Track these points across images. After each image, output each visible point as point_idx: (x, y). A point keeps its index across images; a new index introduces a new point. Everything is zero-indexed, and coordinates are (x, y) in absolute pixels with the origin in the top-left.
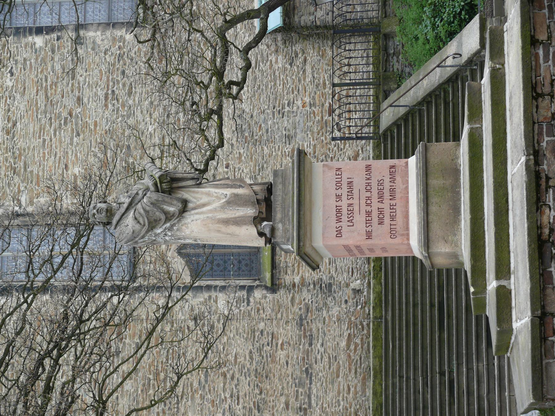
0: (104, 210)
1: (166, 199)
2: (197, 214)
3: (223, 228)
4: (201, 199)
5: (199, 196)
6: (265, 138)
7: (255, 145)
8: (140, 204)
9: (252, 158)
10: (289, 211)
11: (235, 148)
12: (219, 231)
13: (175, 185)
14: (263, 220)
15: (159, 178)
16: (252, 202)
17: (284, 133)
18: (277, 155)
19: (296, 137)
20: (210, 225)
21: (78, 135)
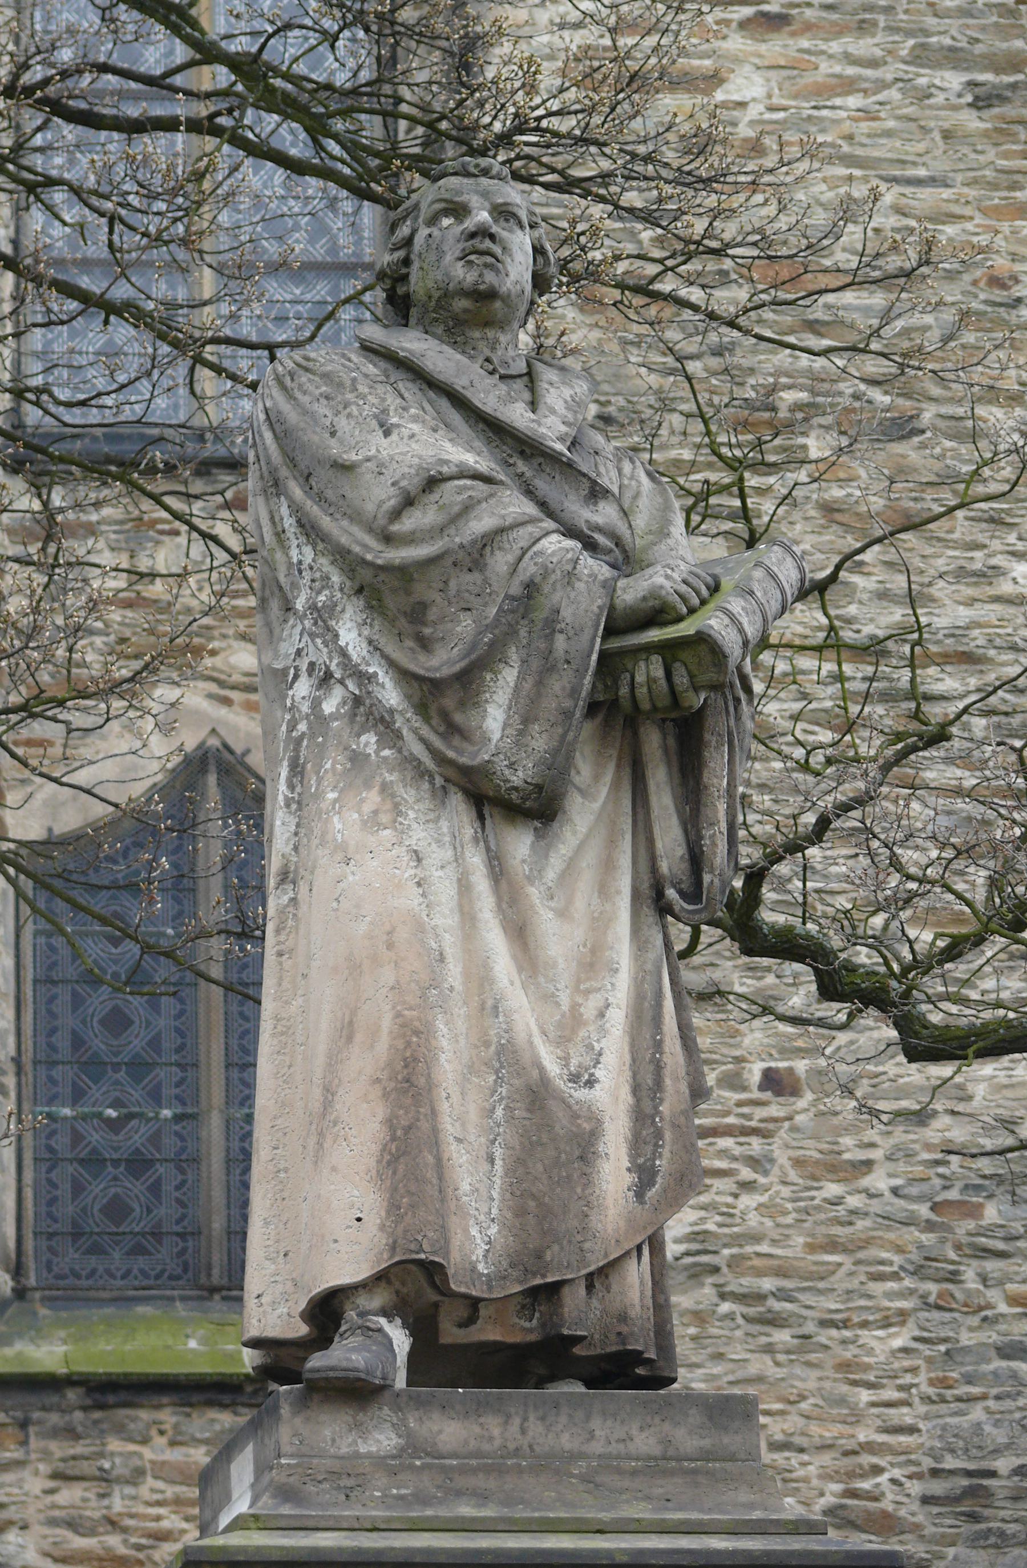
0: (490, 277)
1: (558, 685)
2: (464, 887)
3: (367, 1061)
4: (563, 914)
5: (580, 904)
6: (966, 1339)
7: (918, 1272)
8: (531, 509)
9: (832, 1245)
10: (482, 1497)
11: (900, 1135)
12: (346, 1032)
13: (653, 741)
14: (423, 1330)
15: (702, 639)
16: (539, 1255)
17: (1003, 1465)
18: (856, 1418)
19: (975, 1541)
20: (388, 976)
21: (983, 100)
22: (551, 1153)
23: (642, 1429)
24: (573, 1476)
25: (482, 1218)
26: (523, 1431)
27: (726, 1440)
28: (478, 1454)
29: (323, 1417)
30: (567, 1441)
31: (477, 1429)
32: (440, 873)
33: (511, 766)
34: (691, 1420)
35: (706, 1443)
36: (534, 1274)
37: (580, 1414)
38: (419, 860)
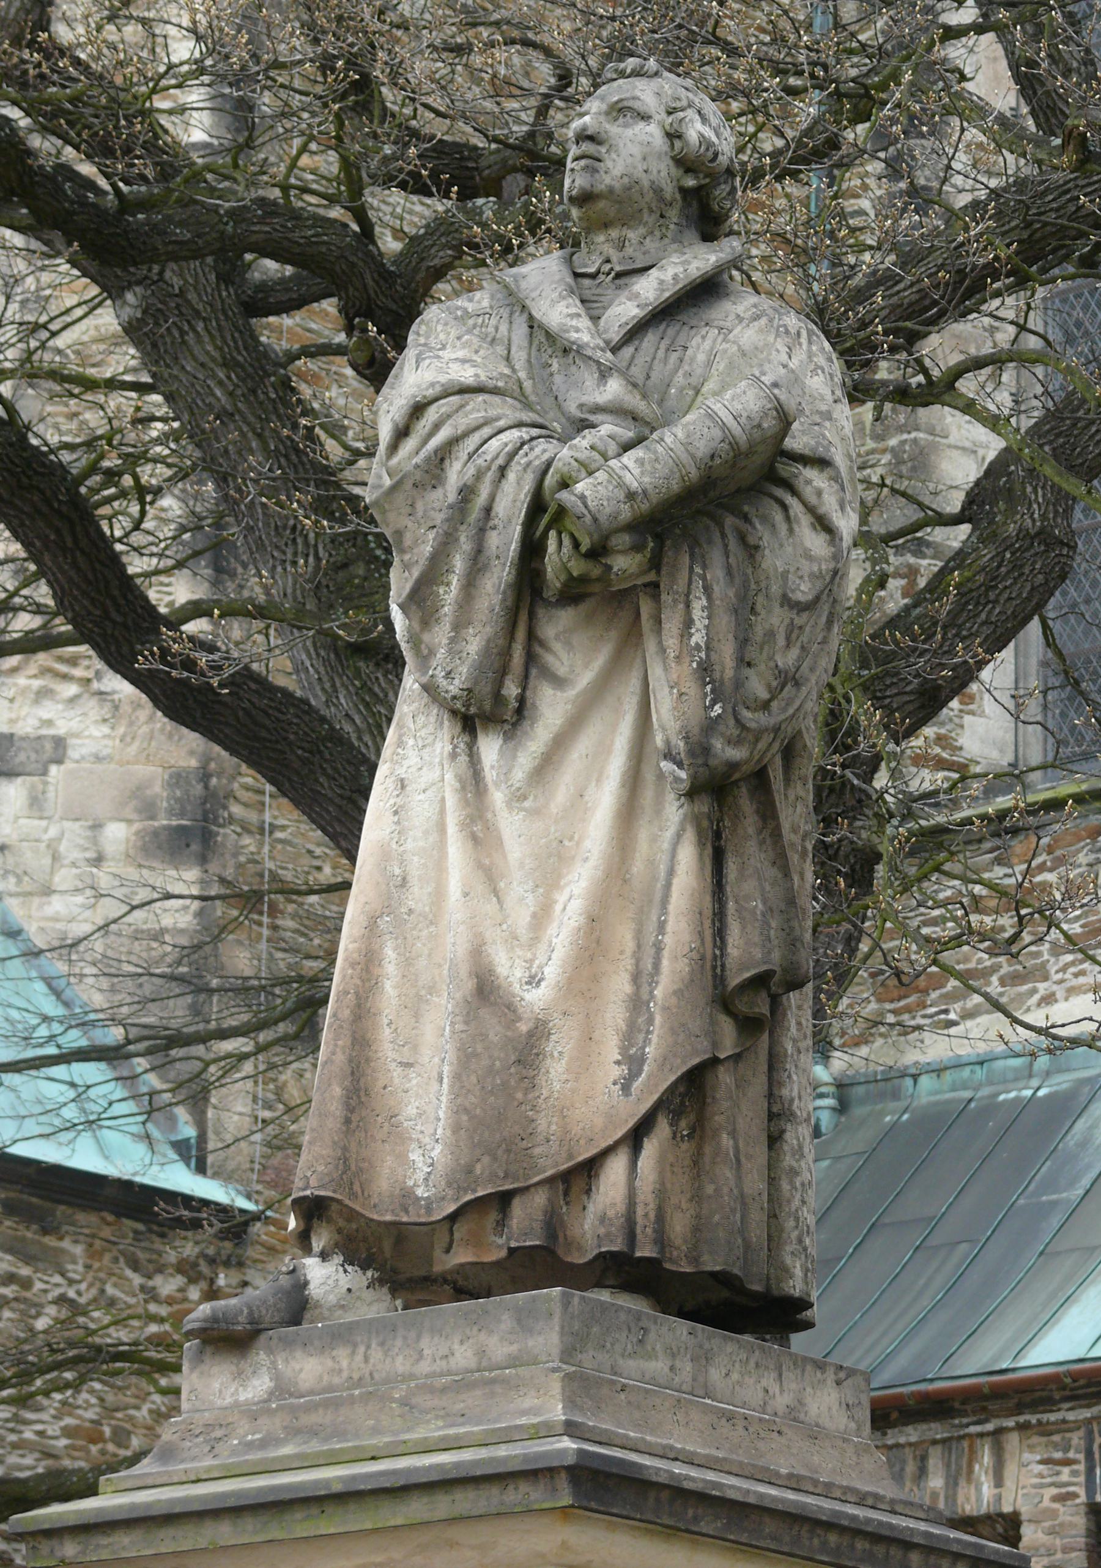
22: (486, 1062)
23: (462, 1342)
24: (394, 1400)
25: (427, 1140)
26: (366, 1359)
27: (531, 1343)
28: (330, 1389)
29: (215, 1370)
30: (401, 1365)
31: (330, 1363)
32: (422, 797)
33: (448, 675)
34: (503, 1326)
35: (514, 1348)
36: (466, 1191)
37: (413, 1334)
38: (403, 787)
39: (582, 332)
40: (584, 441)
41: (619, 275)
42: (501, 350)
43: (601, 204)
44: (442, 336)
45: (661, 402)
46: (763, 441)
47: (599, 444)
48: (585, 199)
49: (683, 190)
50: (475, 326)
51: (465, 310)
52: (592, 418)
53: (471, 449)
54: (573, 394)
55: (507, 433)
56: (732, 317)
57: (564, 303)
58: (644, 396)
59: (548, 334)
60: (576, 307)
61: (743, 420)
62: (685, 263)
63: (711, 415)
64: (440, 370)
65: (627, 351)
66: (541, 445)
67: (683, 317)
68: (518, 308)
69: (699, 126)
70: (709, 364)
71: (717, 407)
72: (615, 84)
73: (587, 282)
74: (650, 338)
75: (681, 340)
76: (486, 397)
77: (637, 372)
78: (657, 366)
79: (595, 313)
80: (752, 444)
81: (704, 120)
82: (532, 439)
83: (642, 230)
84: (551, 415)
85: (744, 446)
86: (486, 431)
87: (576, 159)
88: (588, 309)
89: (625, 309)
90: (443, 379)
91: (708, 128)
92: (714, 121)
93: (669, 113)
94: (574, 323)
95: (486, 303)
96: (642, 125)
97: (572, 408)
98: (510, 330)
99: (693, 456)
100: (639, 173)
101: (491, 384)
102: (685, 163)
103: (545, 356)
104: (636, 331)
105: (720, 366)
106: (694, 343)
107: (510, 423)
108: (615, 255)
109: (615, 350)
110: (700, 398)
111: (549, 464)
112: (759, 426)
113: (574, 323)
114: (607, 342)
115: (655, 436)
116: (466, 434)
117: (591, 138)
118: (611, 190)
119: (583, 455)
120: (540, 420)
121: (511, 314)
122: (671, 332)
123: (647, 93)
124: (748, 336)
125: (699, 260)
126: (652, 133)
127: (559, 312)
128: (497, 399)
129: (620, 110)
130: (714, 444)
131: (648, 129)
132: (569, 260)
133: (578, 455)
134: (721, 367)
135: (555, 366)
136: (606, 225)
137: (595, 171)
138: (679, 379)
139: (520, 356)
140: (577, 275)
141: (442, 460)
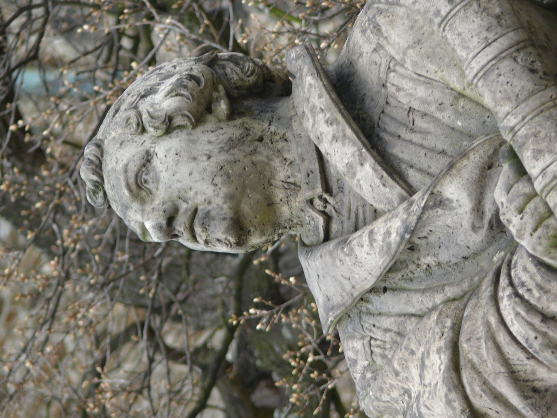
39: (390, 229)
40: (514, 223)
41: (327, 189)
42: (410, 325)
43: (246, 208)
44: (395, 394)
45: (471, 137)
46: (516, 13)
47: (518, 203)
48: (239, 228)
49: (232, 115)
50: (384, 356)
51: (366, 369)
52: (488, 216)
53: (522, 356)
54: (461, 238)
55: (505, 313)
56: (376, 57)
57: (357, 250)
58: (464, 155)
59: (392, 269)
60: (363, 235)
61: (491, 36)
62: (314, 111)
63: (485, 73)
64: (433, 394)
65: (413, 177)
66: (519, 274)
67: (375, 114)
68: (364, 306)
69: (158, 97)
70: (429, 82)
71: (476, 66)
72: (110, 193)
73: (335, 227)
74: (399, 151)
75: (401, 115)
76: (463, 339)
77: (437, 165)
78: (430, 142)
79: (369, 215)
80: (520, 26)
81: (152, 91)
82: (511, 284)
83: (276, 163)
84: (484, 264)
85: (521, 35)
86: (502, 338)
87: (194, 238)
88: (365, 224)
89: (365, 180)
90: (442, 390)
91: (159, 89)
92: (154, 79)
93: (144, 130)
94: (379, 238)
95: (358, 345)
96: (156, 162)
97: (476, 239)
98: (388, 315)
99: (532, 93)
100: (210, 166)
101: (448, 334)
102: (201, 113)
103: (419, 273)
104: (391, 167)
105: (431, 69)
106: (404, 100)
107: (492, 310)
108: (305, 194)
109: (411, 190)
110: (468, 92)
111: (540, 264)
112: (498, 17)
113: (379, 238)
114: (403, 199)
115: (508, 137)
116: (505, 362)
117: (171, 220)
118: (230, 197)
119: (529, 221)
120: (490, 276)
121: (370, 314)
122: (391, 127)
123: (120, 157)
124: (397, 37)
125: (311, 95)
126: (165, 150)
127: (366, 257)
128: (466, 327)
129: (139, 187)
130: (518, 69)
131: (161, 154)
132: (309, 248)
133: (529, 229)
134: (432, 67)
135: (429, 260)
136: (270, 204)
137: (207, 215)
138: (446, 116)
139: (418, 302)
140: (327, 238)
141: (535, 390)
